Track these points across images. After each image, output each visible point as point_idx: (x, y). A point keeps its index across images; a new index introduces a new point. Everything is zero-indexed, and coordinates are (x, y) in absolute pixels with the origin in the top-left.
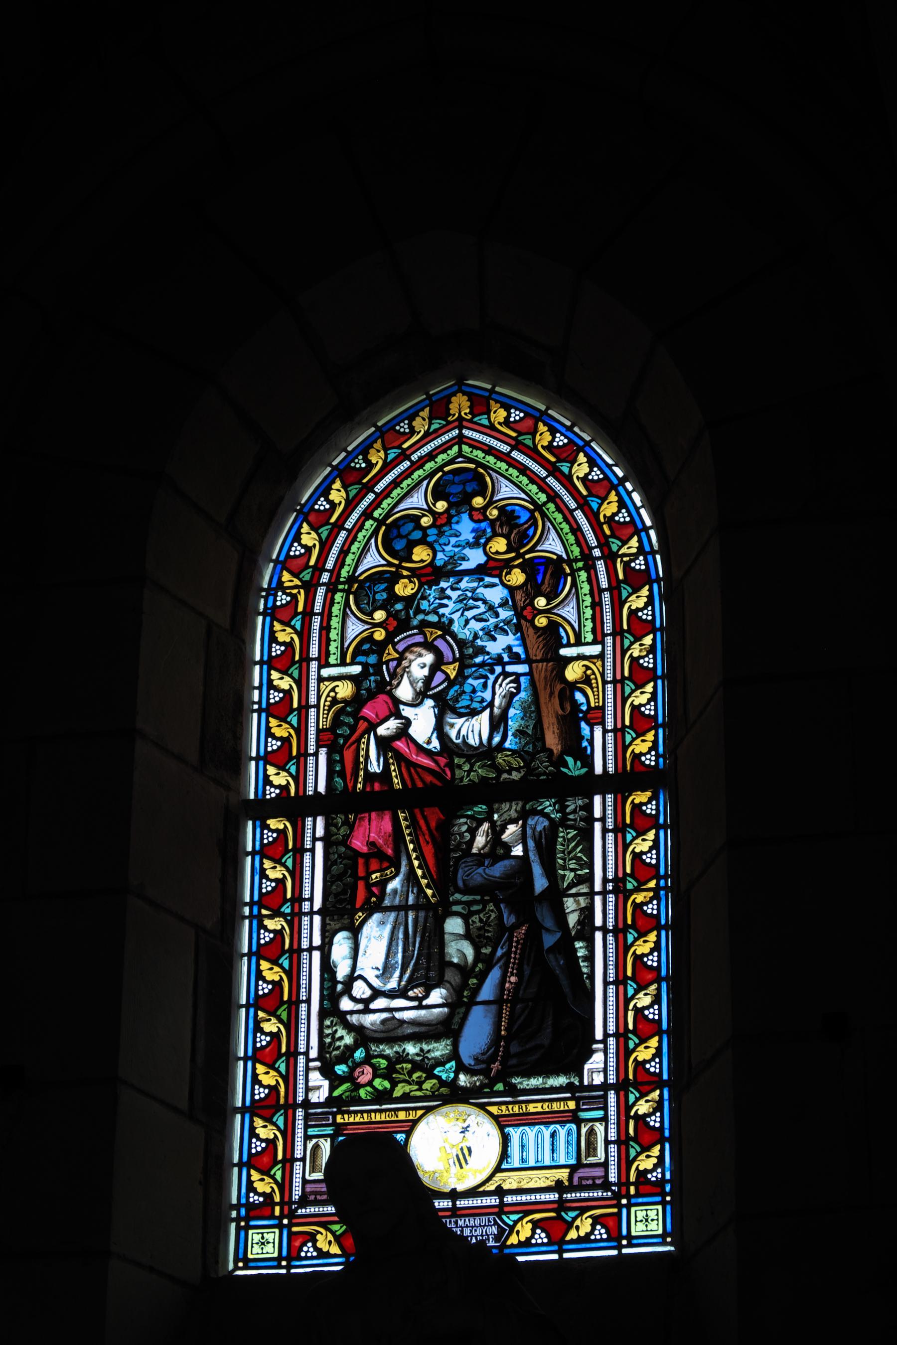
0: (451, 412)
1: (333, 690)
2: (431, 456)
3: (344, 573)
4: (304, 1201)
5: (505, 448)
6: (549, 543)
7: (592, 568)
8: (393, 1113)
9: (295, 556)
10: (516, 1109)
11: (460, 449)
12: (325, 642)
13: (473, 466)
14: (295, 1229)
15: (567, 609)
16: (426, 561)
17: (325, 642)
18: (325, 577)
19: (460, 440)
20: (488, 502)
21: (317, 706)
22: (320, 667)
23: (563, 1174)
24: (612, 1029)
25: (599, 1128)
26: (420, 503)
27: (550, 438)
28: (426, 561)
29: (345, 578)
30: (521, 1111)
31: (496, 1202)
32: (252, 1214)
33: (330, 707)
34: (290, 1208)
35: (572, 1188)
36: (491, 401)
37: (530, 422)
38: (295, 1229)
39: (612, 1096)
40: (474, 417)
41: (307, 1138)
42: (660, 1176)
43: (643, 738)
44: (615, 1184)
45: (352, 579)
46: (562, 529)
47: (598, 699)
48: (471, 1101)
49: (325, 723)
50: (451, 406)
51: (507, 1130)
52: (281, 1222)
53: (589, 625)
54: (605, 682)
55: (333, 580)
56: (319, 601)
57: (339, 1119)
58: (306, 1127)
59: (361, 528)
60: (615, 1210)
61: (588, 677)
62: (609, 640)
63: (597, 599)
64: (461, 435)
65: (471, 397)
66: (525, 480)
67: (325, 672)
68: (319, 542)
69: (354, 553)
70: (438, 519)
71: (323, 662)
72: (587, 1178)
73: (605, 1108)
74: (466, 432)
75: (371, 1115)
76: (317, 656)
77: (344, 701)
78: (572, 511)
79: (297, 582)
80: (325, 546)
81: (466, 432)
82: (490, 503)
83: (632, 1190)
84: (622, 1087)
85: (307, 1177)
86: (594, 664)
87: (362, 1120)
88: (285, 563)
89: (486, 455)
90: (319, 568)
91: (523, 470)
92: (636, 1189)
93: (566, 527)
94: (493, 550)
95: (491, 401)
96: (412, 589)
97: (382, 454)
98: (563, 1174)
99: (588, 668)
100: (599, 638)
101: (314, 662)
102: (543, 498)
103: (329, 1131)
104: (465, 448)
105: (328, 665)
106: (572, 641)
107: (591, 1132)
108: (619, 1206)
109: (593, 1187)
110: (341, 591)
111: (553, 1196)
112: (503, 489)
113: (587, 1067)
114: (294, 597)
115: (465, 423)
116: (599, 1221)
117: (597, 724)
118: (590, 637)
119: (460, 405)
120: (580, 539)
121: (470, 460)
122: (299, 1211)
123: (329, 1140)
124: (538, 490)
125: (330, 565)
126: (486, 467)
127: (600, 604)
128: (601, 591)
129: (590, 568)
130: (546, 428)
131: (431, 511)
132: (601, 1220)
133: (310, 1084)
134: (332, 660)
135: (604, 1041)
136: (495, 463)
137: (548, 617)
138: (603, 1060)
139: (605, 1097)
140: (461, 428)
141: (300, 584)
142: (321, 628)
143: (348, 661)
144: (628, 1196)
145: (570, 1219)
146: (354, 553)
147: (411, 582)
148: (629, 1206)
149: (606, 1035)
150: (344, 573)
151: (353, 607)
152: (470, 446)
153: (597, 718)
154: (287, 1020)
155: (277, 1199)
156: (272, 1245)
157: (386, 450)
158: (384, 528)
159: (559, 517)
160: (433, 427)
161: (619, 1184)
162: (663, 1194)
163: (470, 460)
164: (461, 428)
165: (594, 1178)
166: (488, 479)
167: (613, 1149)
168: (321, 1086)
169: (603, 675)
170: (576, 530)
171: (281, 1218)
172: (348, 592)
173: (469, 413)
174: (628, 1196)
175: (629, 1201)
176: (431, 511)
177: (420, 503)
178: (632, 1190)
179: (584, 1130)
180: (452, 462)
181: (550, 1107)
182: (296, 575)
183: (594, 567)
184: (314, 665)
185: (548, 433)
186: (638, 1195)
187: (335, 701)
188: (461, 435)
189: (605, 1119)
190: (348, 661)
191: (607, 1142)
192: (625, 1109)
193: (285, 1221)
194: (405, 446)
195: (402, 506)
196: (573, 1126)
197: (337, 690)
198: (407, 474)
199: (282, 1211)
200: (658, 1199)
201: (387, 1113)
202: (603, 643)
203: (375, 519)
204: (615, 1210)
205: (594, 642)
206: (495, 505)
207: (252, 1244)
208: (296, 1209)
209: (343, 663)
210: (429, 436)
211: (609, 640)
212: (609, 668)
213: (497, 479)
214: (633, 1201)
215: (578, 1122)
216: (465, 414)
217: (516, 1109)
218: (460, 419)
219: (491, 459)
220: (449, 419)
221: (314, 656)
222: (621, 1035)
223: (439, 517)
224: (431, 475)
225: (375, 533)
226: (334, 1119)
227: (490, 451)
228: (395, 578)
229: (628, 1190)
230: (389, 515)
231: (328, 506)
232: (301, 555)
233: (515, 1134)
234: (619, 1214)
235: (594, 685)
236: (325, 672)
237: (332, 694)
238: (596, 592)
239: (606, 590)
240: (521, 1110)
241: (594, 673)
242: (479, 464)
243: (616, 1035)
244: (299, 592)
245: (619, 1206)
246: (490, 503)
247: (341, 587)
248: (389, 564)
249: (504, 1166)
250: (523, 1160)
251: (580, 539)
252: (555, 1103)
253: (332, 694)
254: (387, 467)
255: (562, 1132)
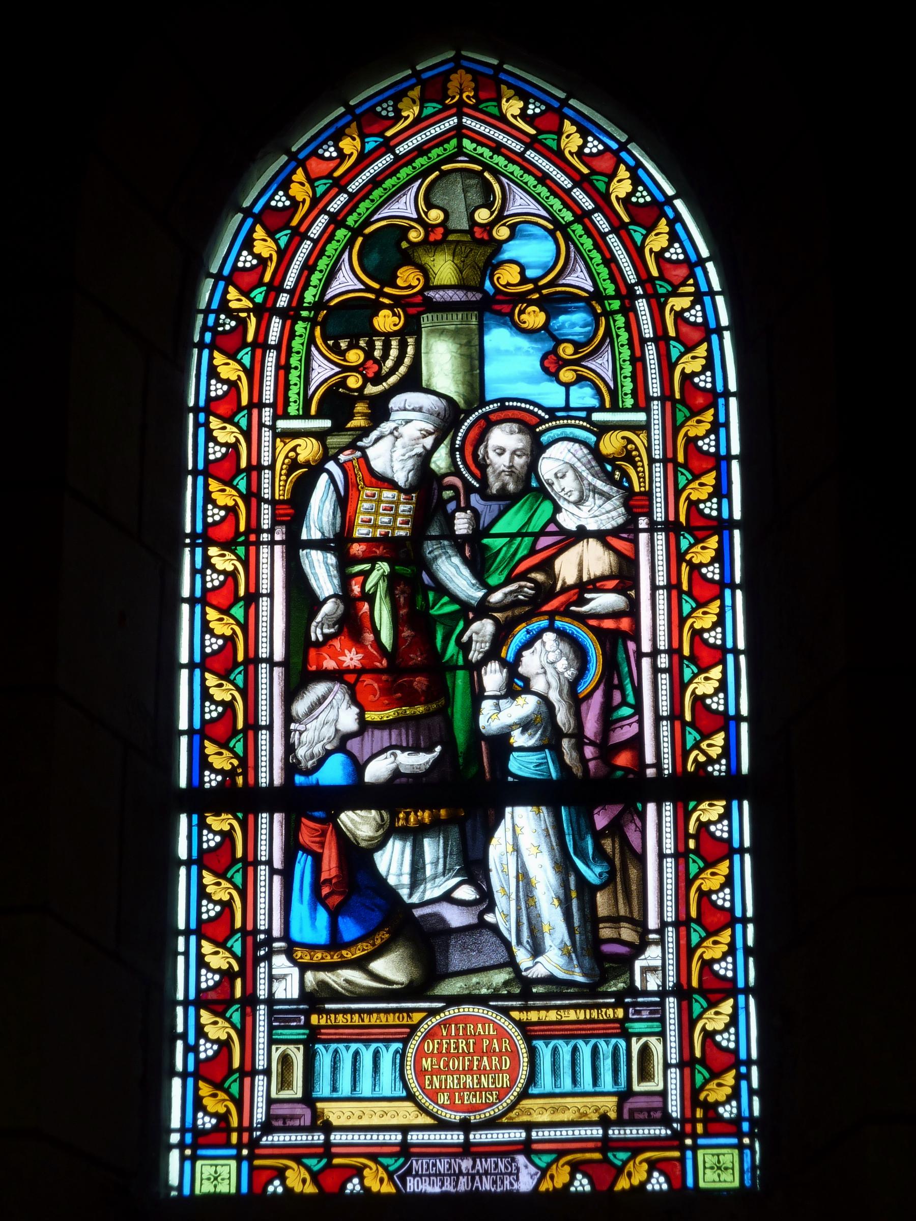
0: (450, 93)
1: (294, 449)
2: (421, 150)
3: (310, 296)
4: (268, 1128)
5: (518, 147)
6: (576, 275)
7: (631, 311)
8: (405, 1015)
9: (244, 269)
10: (595, 1014)
11: (460, 146)
12: (283, 386)
13: (478, 168)
14: (257, 1162)
15: (600, 361)
16: (414, 287)
17: (283, 386)
18: (284, 299)
19: (460, 131)
20: (496, 217)
21: (272, 467)
22: (275, 417)
23: (609, 1105)
24: (670, 916)
25: (655, 1045)
26: (409, 211)
27: (580, 142)
28: (414, 287)
29: (309, 303)
30: (329, 1023)
31: (458, 1139)
32: (201, 1140)
33: (288, 475)
34: (251, 1135)
35: (620, 1122)
36: (502, 86)
37: (553, 118)
38: (257, 1162)
39: (671, 1003)
40: (479, 102)
41: (271, 1042)
42: (735, 1111)
43: (705, 609)
44: (676, 1120)
45: (319, 305)
46: (591, 259)
47: (644, 482)
48: (491, 1003)
49: (281, 492)
50: (450, 85)
51: (535, 1043)
52: (239, 1152)
53: (628, 386)
54: (652, 461)
55: (294, 304)
56: (275, 329)
57: (314, 1019)
58: (271, 1028)
59: (331, 238)
60: (677, 1154)
61: (629, 452)
62: (656, 406)
63: (638, 353)
64: (460, 126)
65: (476, 76)
66: (544, 192)
67: (282, 424)
68: (277, 252)
69: (321, 271)
70: (431, 233)
71: (280, 412)
72: (641, 1110)
73: (662, 1020)
74: (467, 121)
75: (602, 1011)
76: (272, 401)
77: (307, 464)
78: (604, 235)
79: (246, 304)
80: (285, 256)
81: (467, 121)
82: (500, 218)
83: (700, 1128)
84: (683, 992)
85: (274, 1095)
86: (638, 436)
87: (378, 1023)
88: (234, 278)
89: (493, 154)
90: (275, 288)
91: (543, 178)
92: (705, 1128)
93: (597, 257)
94: (503, 282)
95: (502, 86)
96: (395, 325)
97: (358, 142)
98: (609, 1105)
99: (630, 441)
100: (642, 403)
101: (267, 409)
102: (568, 216)
103: (302, 1034)
104: (466, 143)
105: (287, 416)
106: (608, 405)
107: (645, 1051)
108: (683, 1148)
109: (650, 1122)
110: (305, 320)
111: (597, 1132)
112: (519, 201)
113: (638, 964)
114: (242, 324)
115: (466, 110)
116: (658, 1166)
117: (643, 515)
118: (629, 402)
119: (461, 85)
120: (616, 274)
121: (473, 160)
122: (264, 1139)
123: (301, 1047)
124: (562, 207)
125: (289, 283)
126: (495, 173)
127: (643, 359)
128: (643, 341)
129: (628, 310)
130: (574, 128)
131: (420, 220)
132: (661, 1165)
133: (274, 972)
134: (292, 410)
135: (661, 931)
136: (506, 166)
137: (345, 360)
138: (660, 955)
139: (662, 1004)
140: (460, 115)
141: (251, 306)
142: (278, 367)
143: (313, 412)
144: (694, 1136)
145: (619, 1163)
146: (321, 271)
147: (394, 314)
148: (695, 1148)
149: (664, 924)
150: (310, 296)
151: (319, 341)
152: (473, 140)
153: (642, 507)
154: (242, 885)
155: (234, 1122)
156: (707, 1165)
157: (363, 136)
158: (360, 240)
159: (588, 243)
160: (427, 112)
161: (683, 1121)
162: (740, 1135)
163: (473, 160)
164: (460, 115)
165: (649, 1110)
166: (496, 187)
167: (674, 1073)
168: (286, 975)
169: (649, 449)
170: (610, 261)
171: (239, 1146)
172: (313, 322)
173: (473, 97)
174: (694, 1136)
175: (695, 1142)
176: (420, 220)
177: (409, 211)
178: (700, 1128)
179: (636, 1046)
180: (451, 159)
181: (401, 1020)
182: (246, 293)
183: (634, 310)
184: (267, 414)
185: (578, 135)
186: (706, 1134)
187: (294, 465)
188: (460, 126)
189: (662, 1034)
190: (313, 412)
191: (667, 1066)
192: (687, 1023)
193: (245, 1152)
194: (389, 134)
195: (385, 212)
196: (622, 1043)
197: (299, 450)
198: (390, 171)
199: (240, 1138)
200: (734, 1141)
201: (397, 1015)
202: (647, 410)
203: (348, 228)
204: (677, 1154)
205: (635, 408)
206: (424, 216)
207: (202, 1179)
208: (260, 1138)
209: (306, 415)
210: (419, 122)
211: (656, 406)
212: (657, 442)
213: (510, 188)
214: (701, 1141)
215: (627, 1036)
216: (468, 97)
217: (595, 1014)
218: (461, 104)
219: (500, 161)
220: (447, 102)
221: (268, 402)
222: (682, 923)
223: (432, 231)
224: (424, 174)
225: (350, 243)
226: (308, 1020)
227: (498, 148)
228: (375, 307)
229: (694, 1128)
230: (367, 222)
231: (288, 203)
232: (253, 267)
233: (544, 1050)
234: (682, 1160)
235: (640, 464)
236: (282, 424)
237: (292, 454)
238: (637, 343)
239: (649, 340)
240: (329, 1021)
241: (637, 449)
242: (487, 167)
243: (677, 924)
244: (249, 317)
245: (683, 1148)
246: (500, 218)
247: (304, 314)
248: (368, 289)
249: (533, 1090)
250: (334, 1089)
251: (616, 274)
252: (582, 1011)
253: (292, 454)
254: (364, 159)
255: (605, 1048)
